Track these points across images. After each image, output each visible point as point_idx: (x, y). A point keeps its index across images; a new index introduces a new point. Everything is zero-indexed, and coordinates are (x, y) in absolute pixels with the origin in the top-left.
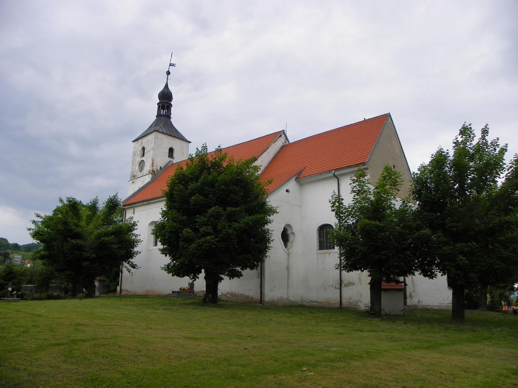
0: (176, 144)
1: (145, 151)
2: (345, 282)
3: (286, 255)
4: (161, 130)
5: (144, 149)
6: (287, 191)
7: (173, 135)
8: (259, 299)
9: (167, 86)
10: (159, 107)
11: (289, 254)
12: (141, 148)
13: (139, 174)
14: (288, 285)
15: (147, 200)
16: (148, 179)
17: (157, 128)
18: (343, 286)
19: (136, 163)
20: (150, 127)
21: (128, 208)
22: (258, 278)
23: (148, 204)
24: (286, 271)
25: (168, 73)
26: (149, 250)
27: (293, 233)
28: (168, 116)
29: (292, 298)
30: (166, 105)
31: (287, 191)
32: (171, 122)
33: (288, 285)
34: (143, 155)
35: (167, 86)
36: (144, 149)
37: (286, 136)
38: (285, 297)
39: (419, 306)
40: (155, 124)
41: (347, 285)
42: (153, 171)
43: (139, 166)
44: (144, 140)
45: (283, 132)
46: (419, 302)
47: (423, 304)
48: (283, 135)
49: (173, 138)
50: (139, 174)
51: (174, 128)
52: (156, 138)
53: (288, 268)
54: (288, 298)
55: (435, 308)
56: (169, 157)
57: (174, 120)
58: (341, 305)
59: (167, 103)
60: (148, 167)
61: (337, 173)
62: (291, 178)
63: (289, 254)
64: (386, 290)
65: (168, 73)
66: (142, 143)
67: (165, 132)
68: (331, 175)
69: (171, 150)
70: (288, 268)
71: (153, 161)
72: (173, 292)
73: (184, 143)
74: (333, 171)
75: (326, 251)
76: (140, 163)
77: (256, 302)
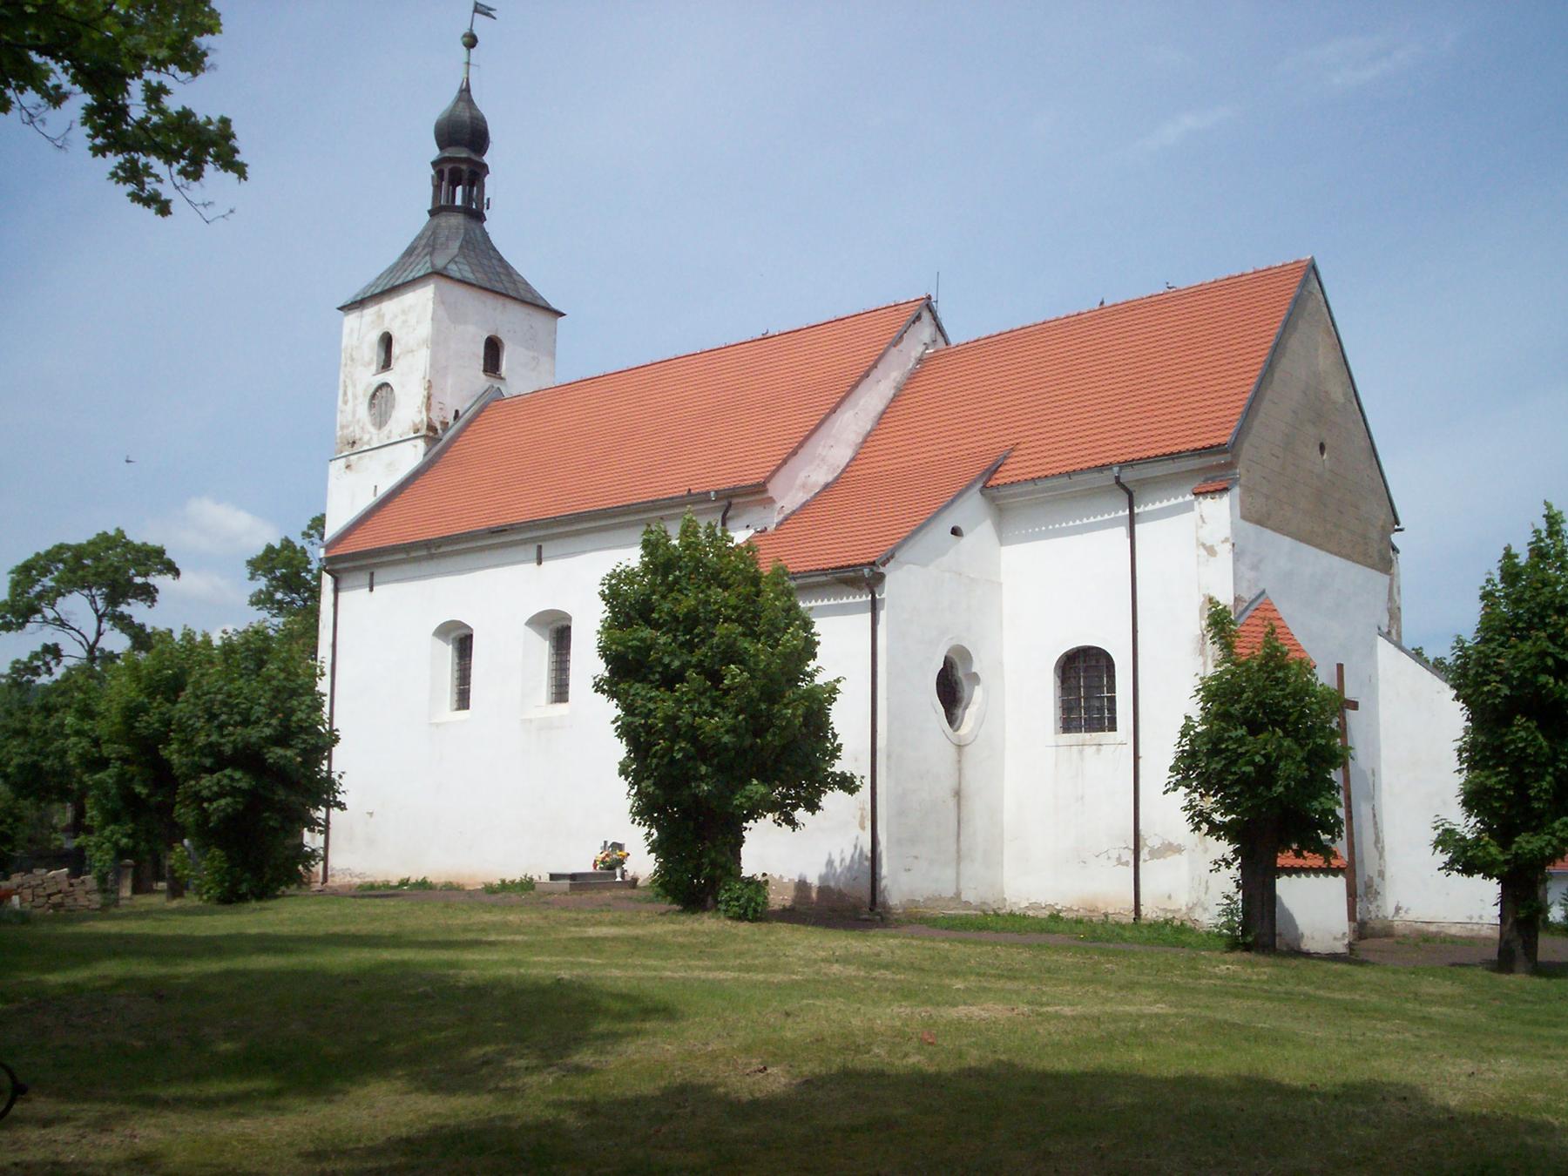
0: (508, 320)
1: (396, 350)
2: (1150, 840)
3: (952, 750)
4: (453, 270)
5: (387, 341)
6: (955, 532)
7: (498, 287)
8: (867, 897)
9: (465, 92)
10: (440, 175)
11: (960, 747)
12: (374, 336)
13: (372, 436)
14: (958, 851)
15: (427, 544)
16: (412, 456)
17: (440, 262)
18: (1144, 854)
19: (360, 389)
20: (410, 252)
21: (346, 570)
22: (863, 828)
23: (431, 557)
24: (952, 803)
25: (471, 41)
26: (438, 725)
27: (975, 678)
28: (475, 213)
29: (969, 895)
31: (955, 532)
32: (485, 235)
33: (958, 851)
34: (386, 365)
35: (465, 92)
36: (387, 341)
37: (935, 318)
38: (949, 892)
39: (1397, 923)
40: (428, 242)
41: (1081, 752)
42: (431, 427)
43: (371, 405)
44: (390, 306)
45: (928, 304)
46: (1398, 909)
47: (1411, 916)
48: (926, 316)
49: (500, 301)
50: (372, 436)
51: (501, 259)
52: (440, 300)
53: (958, 794)
54: (958, 894)
55: (1454, 931)
56: (485, 371)
57: (503, 226)
58: (540, 548)
59: (467, 160)
60: (409, 411)
61: (1128, 476)
62: (968, 487)
63: (960, 747)
64: (1290, 871)
65: (471, 41)
66: (381, 316)
67: (469, 276)
68: (1107, 478)
69: (493, 350)
70: (958, 794)
71: (430, 387)
72: (553, 877)
73: (539, 319)
74: (1116, 469)
75: (1087, 736)
76: (374, 396)
77: (856, 908)
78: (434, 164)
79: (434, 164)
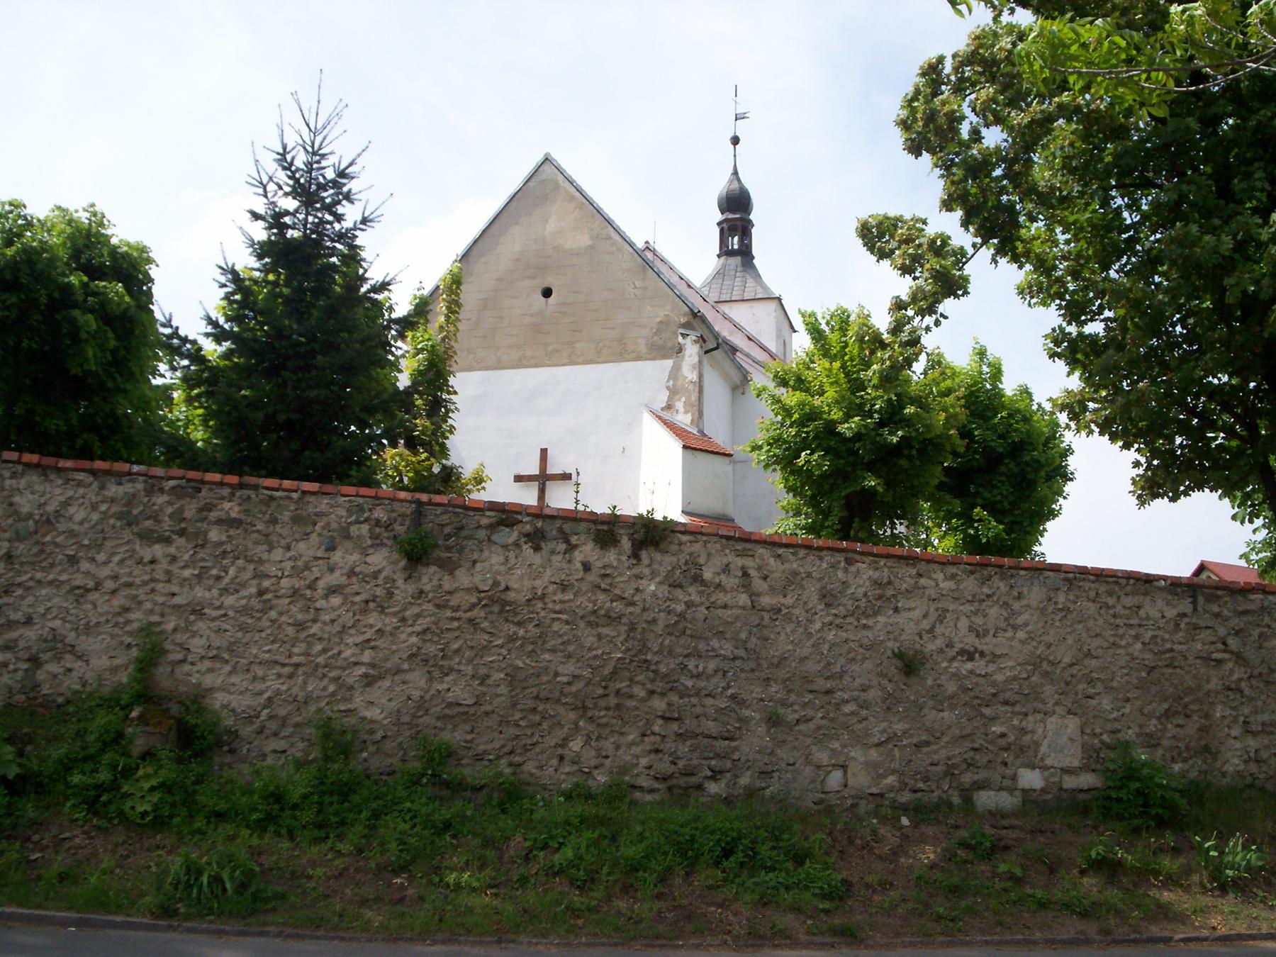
10: (722, 231)
28: (745, 253)
30: (739, 224)
78: (719, 224)
79: (719, 224)
